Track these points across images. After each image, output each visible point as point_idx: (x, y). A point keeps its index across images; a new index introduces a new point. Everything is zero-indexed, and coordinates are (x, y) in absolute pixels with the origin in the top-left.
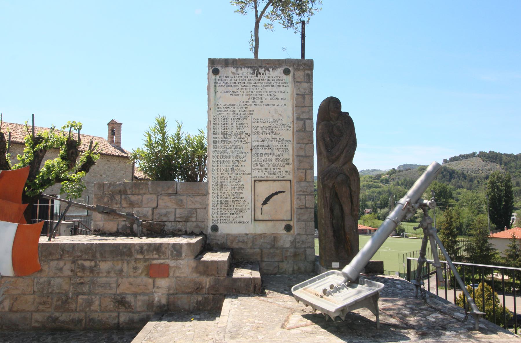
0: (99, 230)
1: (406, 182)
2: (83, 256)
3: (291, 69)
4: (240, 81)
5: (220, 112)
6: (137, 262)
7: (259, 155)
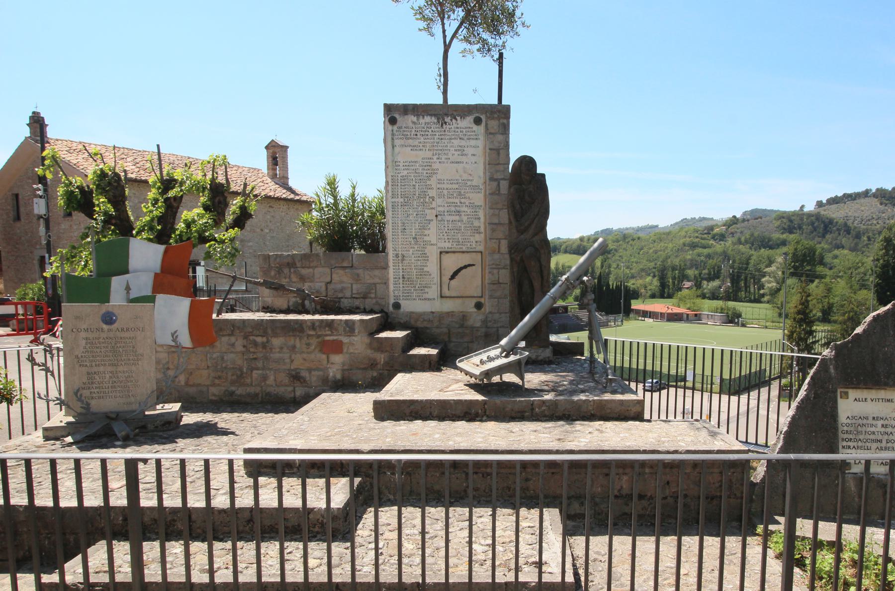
0: (268, 307)
1: (752, 238)
2: (255, 332)
3: (483, 117)
4: (422, 133)
5: (399, 171)
6: (310, 338)
7: (446, 223)
